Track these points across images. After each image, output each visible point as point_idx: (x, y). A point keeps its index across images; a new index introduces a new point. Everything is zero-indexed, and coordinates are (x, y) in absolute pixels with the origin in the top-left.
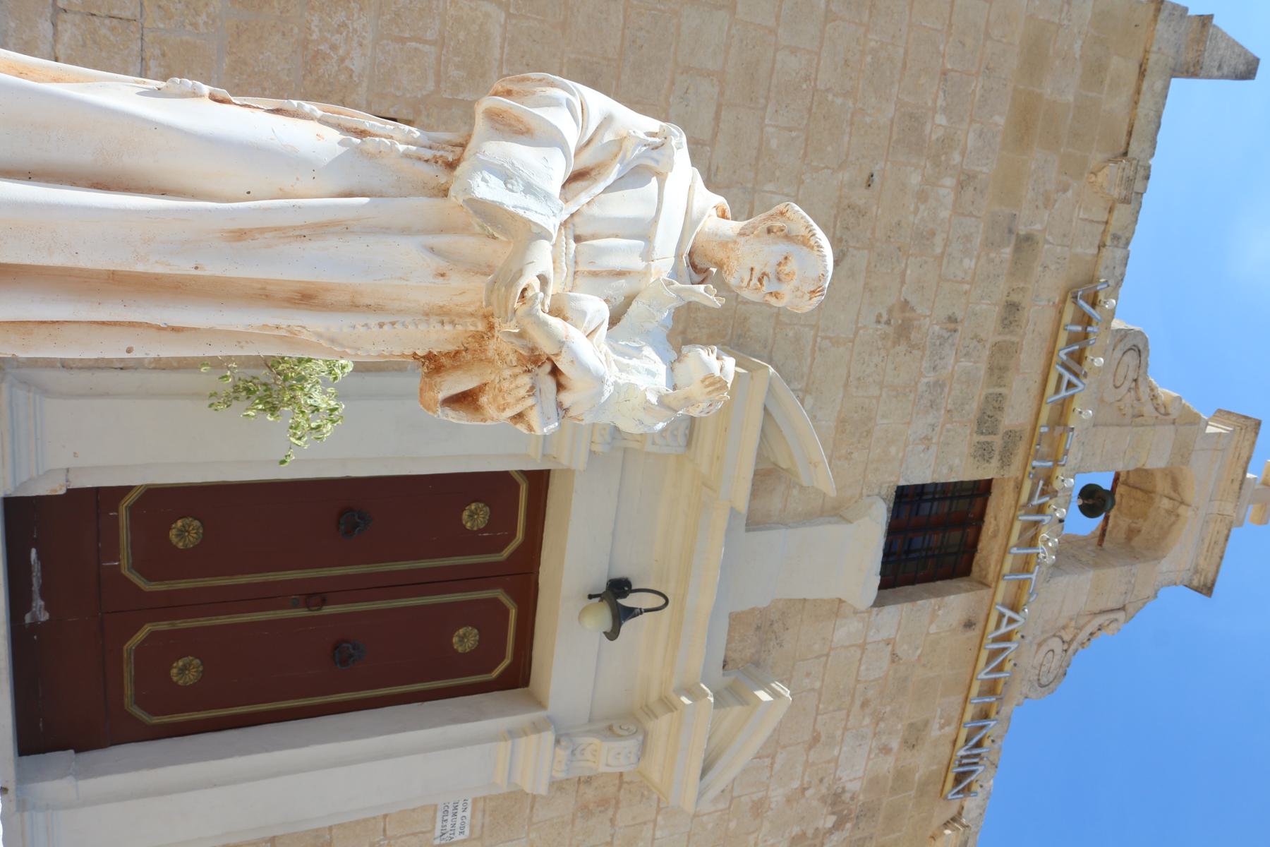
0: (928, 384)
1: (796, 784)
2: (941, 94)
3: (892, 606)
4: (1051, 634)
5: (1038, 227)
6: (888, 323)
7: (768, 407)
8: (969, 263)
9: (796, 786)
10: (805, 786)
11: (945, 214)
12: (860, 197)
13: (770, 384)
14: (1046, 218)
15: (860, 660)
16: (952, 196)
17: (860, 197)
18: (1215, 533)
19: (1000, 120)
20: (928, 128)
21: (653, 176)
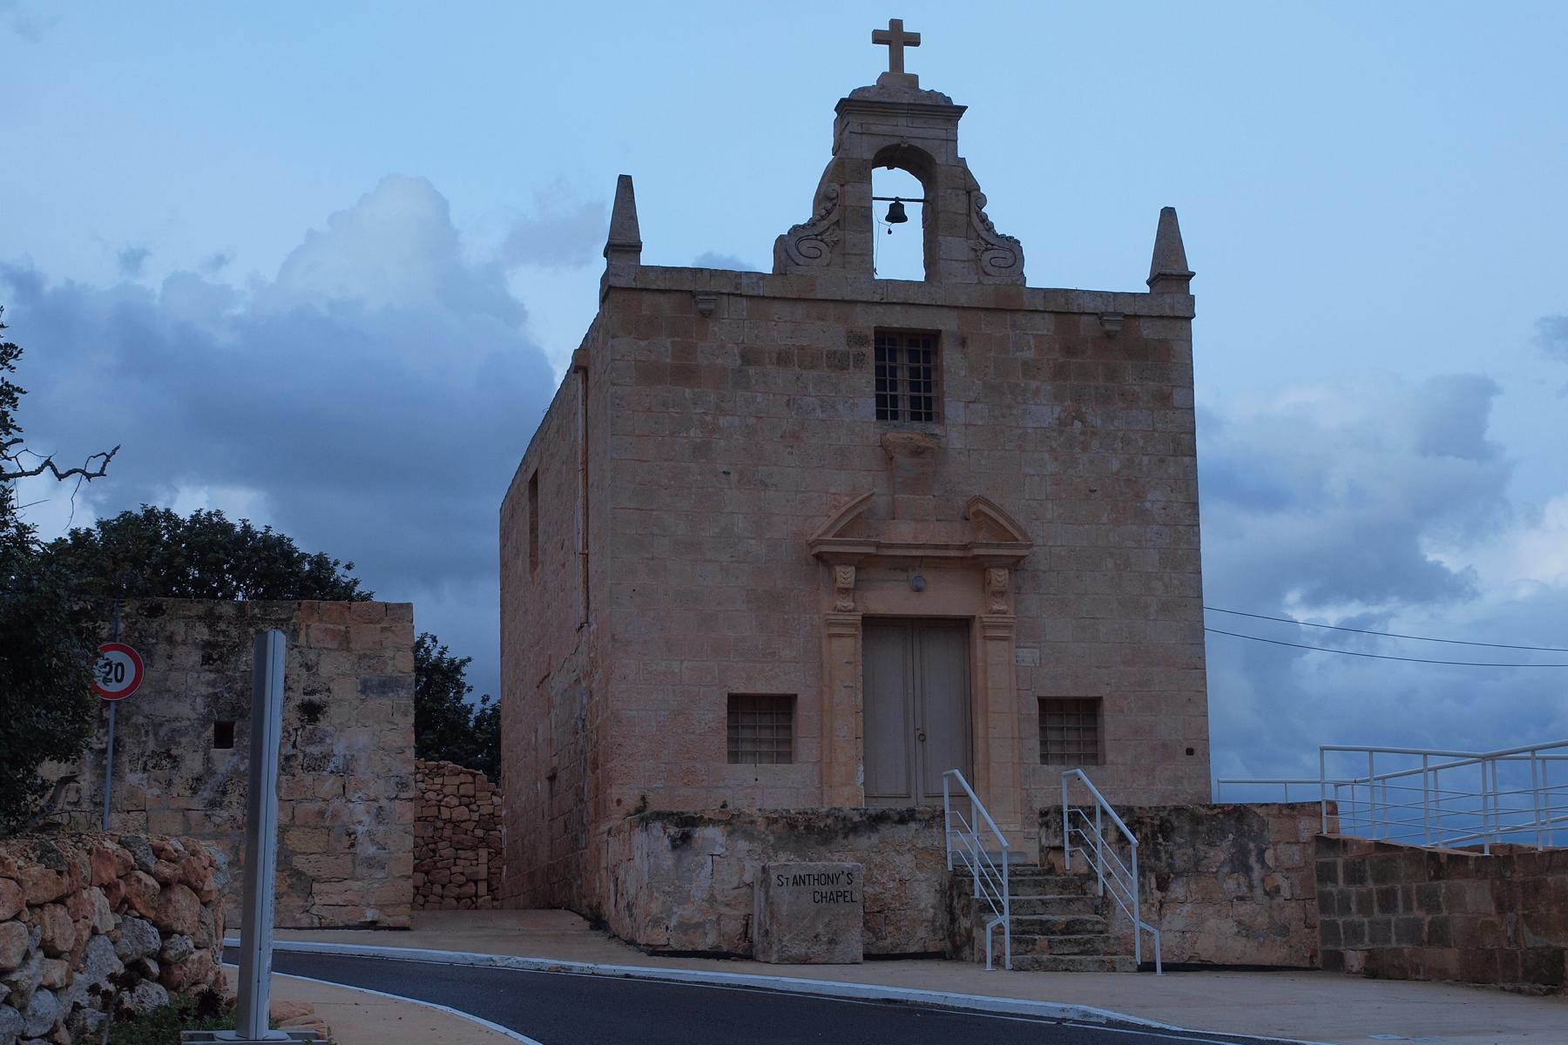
0: (822, 412)
1: (1047, 456)
2: (681, 435)
3: (946, 409)
4: (533, 734)
5: (736, 350)
6: (792, 447)
7: (540, 477)
8: (759, 399)
9: (1048, 456)
10: (1049, 448)
11: (737, 421)
12: (734, 477)
13: (536, 471)
14: (730, 345)
15: (975, 426)
16: (728, 417)
17: (734, 477)
18: (734, 559)
19: (688, 392)
20: (698, 440)
21: (868, 179)
